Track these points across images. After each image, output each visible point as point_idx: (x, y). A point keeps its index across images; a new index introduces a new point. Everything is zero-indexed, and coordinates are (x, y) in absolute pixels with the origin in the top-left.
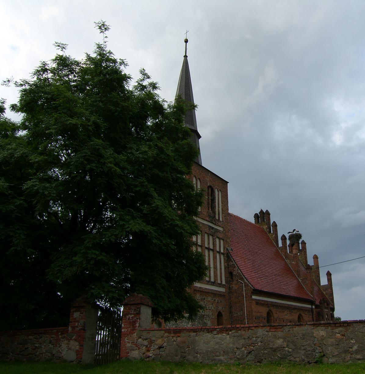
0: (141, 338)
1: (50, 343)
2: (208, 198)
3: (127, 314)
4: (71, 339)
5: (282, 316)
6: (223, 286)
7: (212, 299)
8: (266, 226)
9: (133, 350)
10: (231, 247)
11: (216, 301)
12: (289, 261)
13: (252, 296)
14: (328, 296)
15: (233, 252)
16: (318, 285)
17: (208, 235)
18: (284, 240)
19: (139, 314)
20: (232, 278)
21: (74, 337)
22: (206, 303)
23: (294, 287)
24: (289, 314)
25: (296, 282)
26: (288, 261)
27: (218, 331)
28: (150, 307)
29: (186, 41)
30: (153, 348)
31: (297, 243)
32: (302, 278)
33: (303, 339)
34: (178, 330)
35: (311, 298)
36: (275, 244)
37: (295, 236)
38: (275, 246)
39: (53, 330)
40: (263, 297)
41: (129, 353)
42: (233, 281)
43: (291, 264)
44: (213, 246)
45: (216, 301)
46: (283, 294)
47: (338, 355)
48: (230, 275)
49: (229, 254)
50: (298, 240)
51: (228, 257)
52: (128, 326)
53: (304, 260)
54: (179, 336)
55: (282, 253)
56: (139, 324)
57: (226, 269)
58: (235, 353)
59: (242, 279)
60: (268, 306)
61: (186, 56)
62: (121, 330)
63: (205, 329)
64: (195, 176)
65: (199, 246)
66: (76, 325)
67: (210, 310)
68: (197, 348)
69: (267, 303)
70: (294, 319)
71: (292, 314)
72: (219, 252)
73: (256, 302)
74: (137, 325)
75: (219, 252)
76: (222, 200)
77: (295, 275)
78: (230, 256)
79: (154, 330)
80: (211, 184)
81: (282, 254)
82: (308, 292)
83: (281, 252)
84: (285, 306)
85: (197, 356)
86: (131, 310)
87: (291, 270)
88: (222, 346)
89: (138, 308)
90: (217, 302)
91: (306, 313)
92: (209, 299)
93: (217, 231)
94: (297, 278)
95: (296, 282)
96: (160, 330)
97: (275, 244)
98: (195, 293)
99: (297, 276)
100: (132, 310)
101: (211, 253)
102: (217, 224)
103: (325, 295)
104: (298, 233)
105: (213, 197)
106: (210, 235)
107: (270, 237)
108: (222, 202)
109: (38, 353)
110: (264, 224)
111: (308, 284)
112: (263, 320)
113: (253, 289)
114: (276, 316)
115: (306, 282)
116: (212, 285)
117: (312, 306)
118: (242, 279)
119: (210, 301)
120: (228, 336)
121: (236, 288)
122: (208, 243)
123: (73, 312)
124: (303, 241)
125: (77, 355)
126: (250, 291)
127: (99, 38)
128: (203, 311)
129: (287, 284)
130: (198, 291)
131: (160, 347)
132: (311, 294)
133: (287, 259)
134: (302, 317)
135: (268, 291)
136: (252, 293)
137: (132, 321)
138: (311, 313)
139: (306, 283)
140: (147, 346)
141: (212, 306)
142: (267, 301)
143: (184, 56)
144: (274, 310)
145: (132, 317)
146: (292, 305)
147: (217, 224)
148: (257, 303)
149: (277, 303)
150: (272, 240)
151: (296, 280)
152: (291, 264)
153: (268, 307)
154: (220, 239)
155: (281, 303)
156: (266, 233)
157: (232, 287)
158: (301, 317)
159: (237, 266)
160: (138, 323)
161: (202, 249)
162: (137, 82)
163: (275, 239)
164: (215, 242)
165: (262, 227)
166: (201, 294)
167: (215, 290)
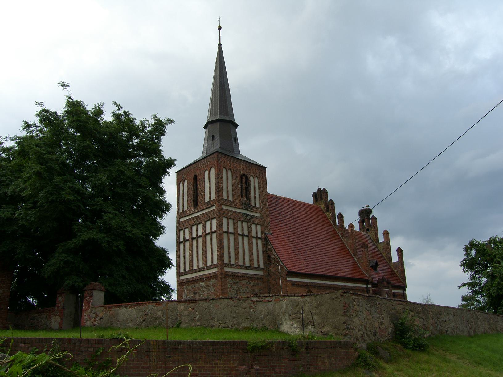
0: (92, 313)
1: (46, 318)
2: (242, 186)
4: (57, 315)
6: (261, 269)
7: (247, 283)
8: (324, 205)
9: (87, 321)
10: (271, 231)
11: (252, 284)
12: (345, 240)
15: (273, 236)
16: (389, 262)
17: (242, 222)
18: (340, 218)
19: (92, 296)
20: (270, 262)
21: (58, 314)
22: (239, 287)
25: (352, 262)
26: (344, 240)
28: (104, 291)
29: (220, 28)
30: (97, 319)
33: (172, 311)
35: (367, 277)
36: (332, 223)
37: (364, 211)
38: (330, 225)
39: (48, 309)
41: (85, 323)
42: (271, 264)
44: (248, 232)
45: (252, 284)
46: (326, 275)
47: (187, 322)
48: (268, 258)
49: (267, 238)
51: (266, 241)
53: (375, 237)
54: (111, 311)
57: (265, 253)
58: (137, 321)
59: (278, 262)
61: (220, 45)
62: (82, 307)
64: (225, 168)
65: (231, 233)
66: (60, 305)
67: (244, 292)
68: (118, 318)
69: (306, 284)
72: (256, 238)
73: (292, 284)
74: (91, 304)
75: (256, 238)
76: (259, 186)
78: (268, 240)
79: (98, 307)
80: (244, 172)
84: (329, 286)
85: (118, 324)
88: (131, 316)
89: (91, 292)
90: (254, 285)
92: (244, 282)
93: (253, 217)
95: (352, 262)
97: (332, 223)
98: (226, 278)
99: (353, 255)
101: (246, 239)
102: (253, 210)
103: (395, 273)
104: (368, 207)
105: (248, 185)
106: (244, 221)
107: (327, 215)
108: (259, 189)
109: (40, 325)
110: (322, 203)
113: (287, 272)
115: (361, 261)
116: (246, 269)
118: (278, 262)
119: (243, 284)
120: (134, 310)
121: (274, 271)
122: (242, 230)
123: (58, 296)
124: (373, 216)
125: (59, 325)
126: (285, 273)
127: (66, 92)
128: (236, 294)
130: (230, 275)
131: (101, 318)
132: (366, 273)
133: (344, 237)
135: (306, 272)
136: (287, 275)
139: (361, 262)
140: (94, 318)
141: (246, 288)
142: (306, 282)
143: (218, 45)
147: (253, 210)
148: (293, 284)
149: (319, 283)
150: (330, 219)
152: (347, 242)
153: (307, 288)
154: (256, 224)
155: (324, 284)
156: (324, 212)
157: (270, 270)
159: (274, 249)
161: (234, 236)
162: (113, 113)
163: (332, 218)
164: (250, 228)
165: (320, 206)
166: (233, 279)
167: (251, 274)
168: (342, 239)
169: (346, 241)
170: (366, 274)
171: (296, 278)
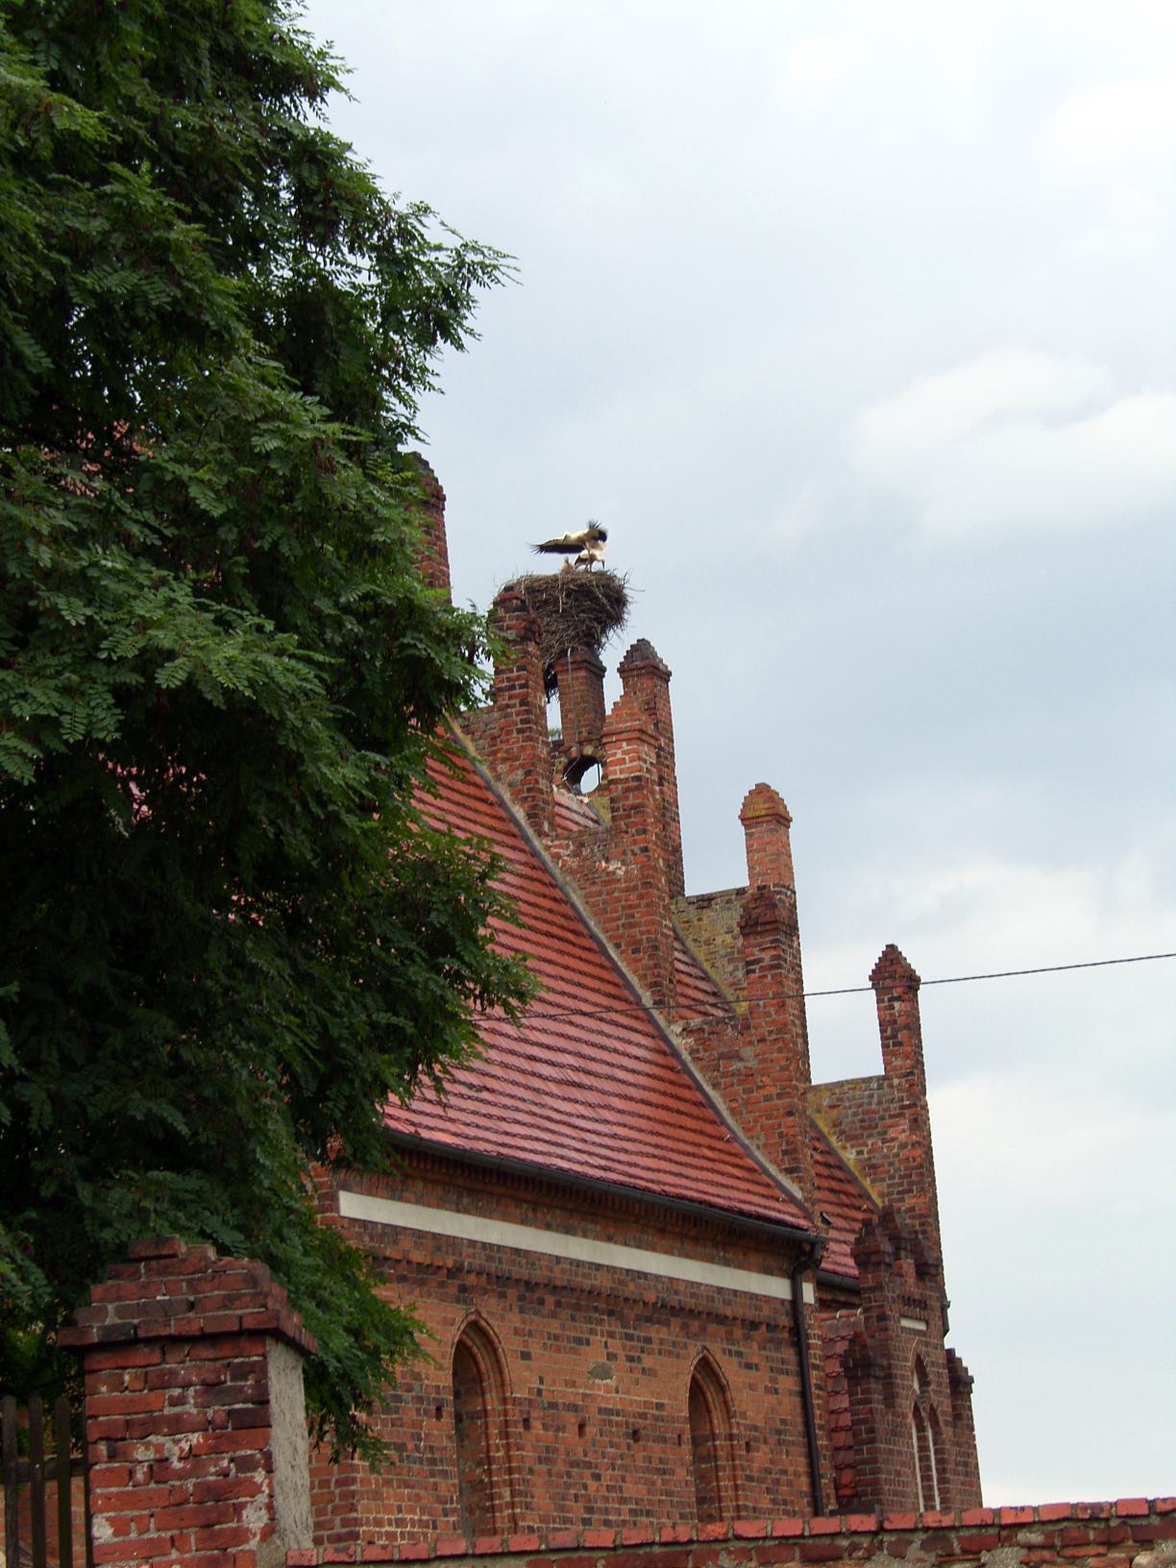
3: (128, 1424)
5: (574, 1384)
13: (335, 1199)
14: (883, 1187)
23: (643, 1102)
24: (622, 1361)
27: (1030, 1547)
31: (578, 665)
32: (696, 1021)
34: (656, 1549)
40: (419, 1201)
43: (587, 875)
50: (592, 641)
52: (153, 1535)
55: (501, 768)
56: (270, 1507)
60: (463, 1289)
63: (914, 1530)
70: (660, 1406)
71: (648, 1361)
77: (629, 986)
81: (498, 778)
82: (758, 1154)
83: (484, 769)
84: (588, 1283)
86: (177, 1392)
87: (593, 937)
89: (240, 1373)
91: (753, 1352)
94: (652, 1021)
96: (482, 1556)
99: (647, 998)
100: (186, 1386)
103: (852, 1180)
111: (764, 1073)
112: (428, 1423)
114: (522, 1378)
117: (796, 1291)
129: (588, 1073)
132: (789, 1171)
134: (722, 1389)
137: (190, 1484)
138: (789, 1354)
142: (452, 1242)
144: (504, 1323)
145: (191, 1455)
146: (645, 1275)
151: (646, 1034)
152: (587, 875)
155: (558, 1259)
158: (711, 1396)
160: (262, 1499)
168: (536, 842)
169: (573, 863)
170: (785, 1181)
171: (395, 1195)
